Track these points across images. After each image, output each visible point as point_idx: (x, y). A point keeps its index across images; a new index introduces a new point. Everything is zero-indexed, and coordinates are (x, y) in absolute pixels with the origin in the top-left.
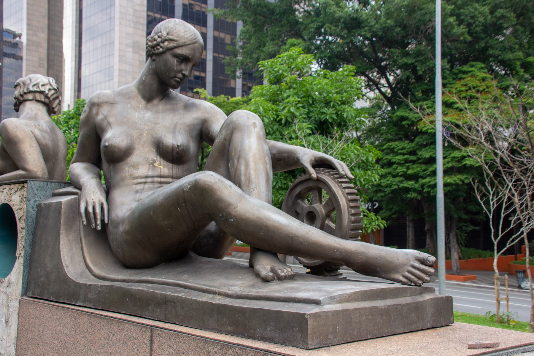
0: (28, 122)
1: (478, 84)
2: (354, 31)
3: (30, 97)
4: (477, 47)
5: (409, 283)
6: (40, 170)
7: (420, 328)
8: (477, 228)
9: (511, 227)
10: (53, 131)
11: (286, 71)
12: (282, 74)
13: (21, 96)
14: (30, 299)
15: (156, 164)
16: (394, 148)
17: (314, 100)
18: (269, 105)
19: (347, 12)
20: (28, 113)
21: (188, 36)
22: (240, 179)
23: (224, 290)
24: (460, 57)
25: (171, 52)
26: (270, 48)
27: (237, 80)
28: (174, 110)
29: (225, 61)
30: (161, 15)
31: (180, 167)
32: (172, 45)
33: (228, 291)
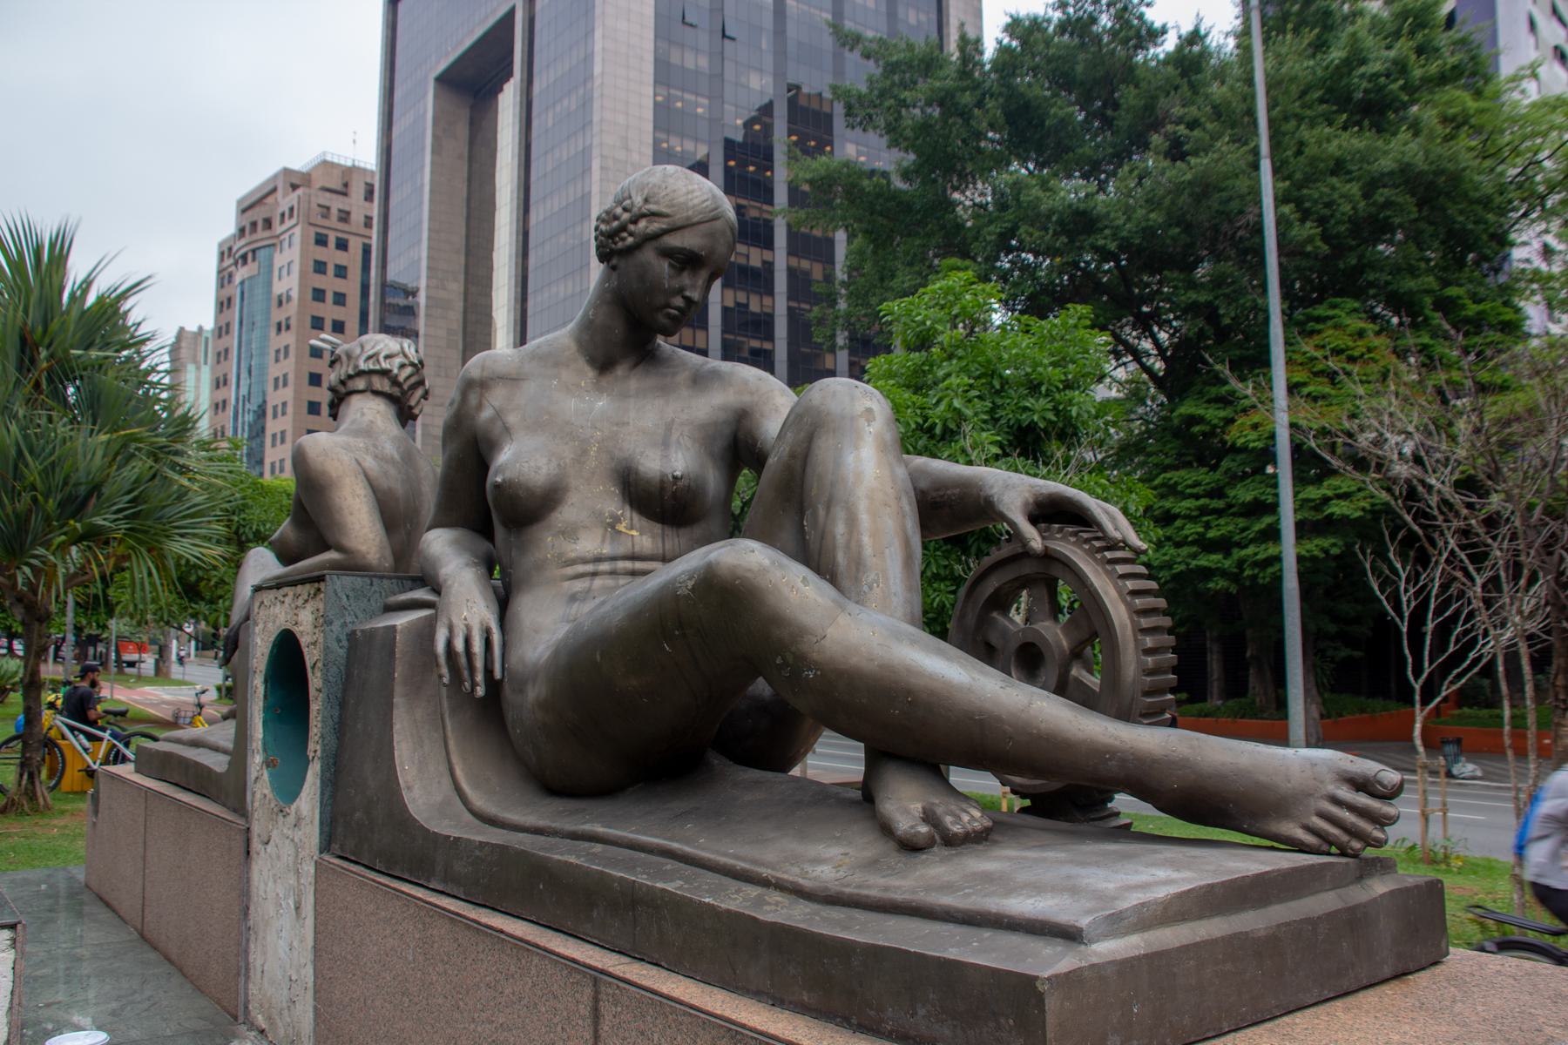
0: (351, 440)
1: (1350, 344)
2: (1082, 238)
3: (360, 384)
4: (1342, 266)
5: (1325, 847)
6: (374, 549)
7: (1365, 982)
8: (1357, 654)
9: (1451, 650)
11: (939, 321)
13: (343, 383)
14: (337, 861)
15: (621, 527)
16: (1176, 484)
17: (1005, 382)
18: (906, 395)
19: (1064, 199)
20: (353, 422)
21: (696, 201)
22: (834, 557)
23: (791, 874)
24: (1324, 279)
25: (654, 244)
26: (904, 278)
27: (839, 353)
28: (665, 391)
29: (813, 315)
31: (683, 531)
32: (656, 226)
33: (801, 881)
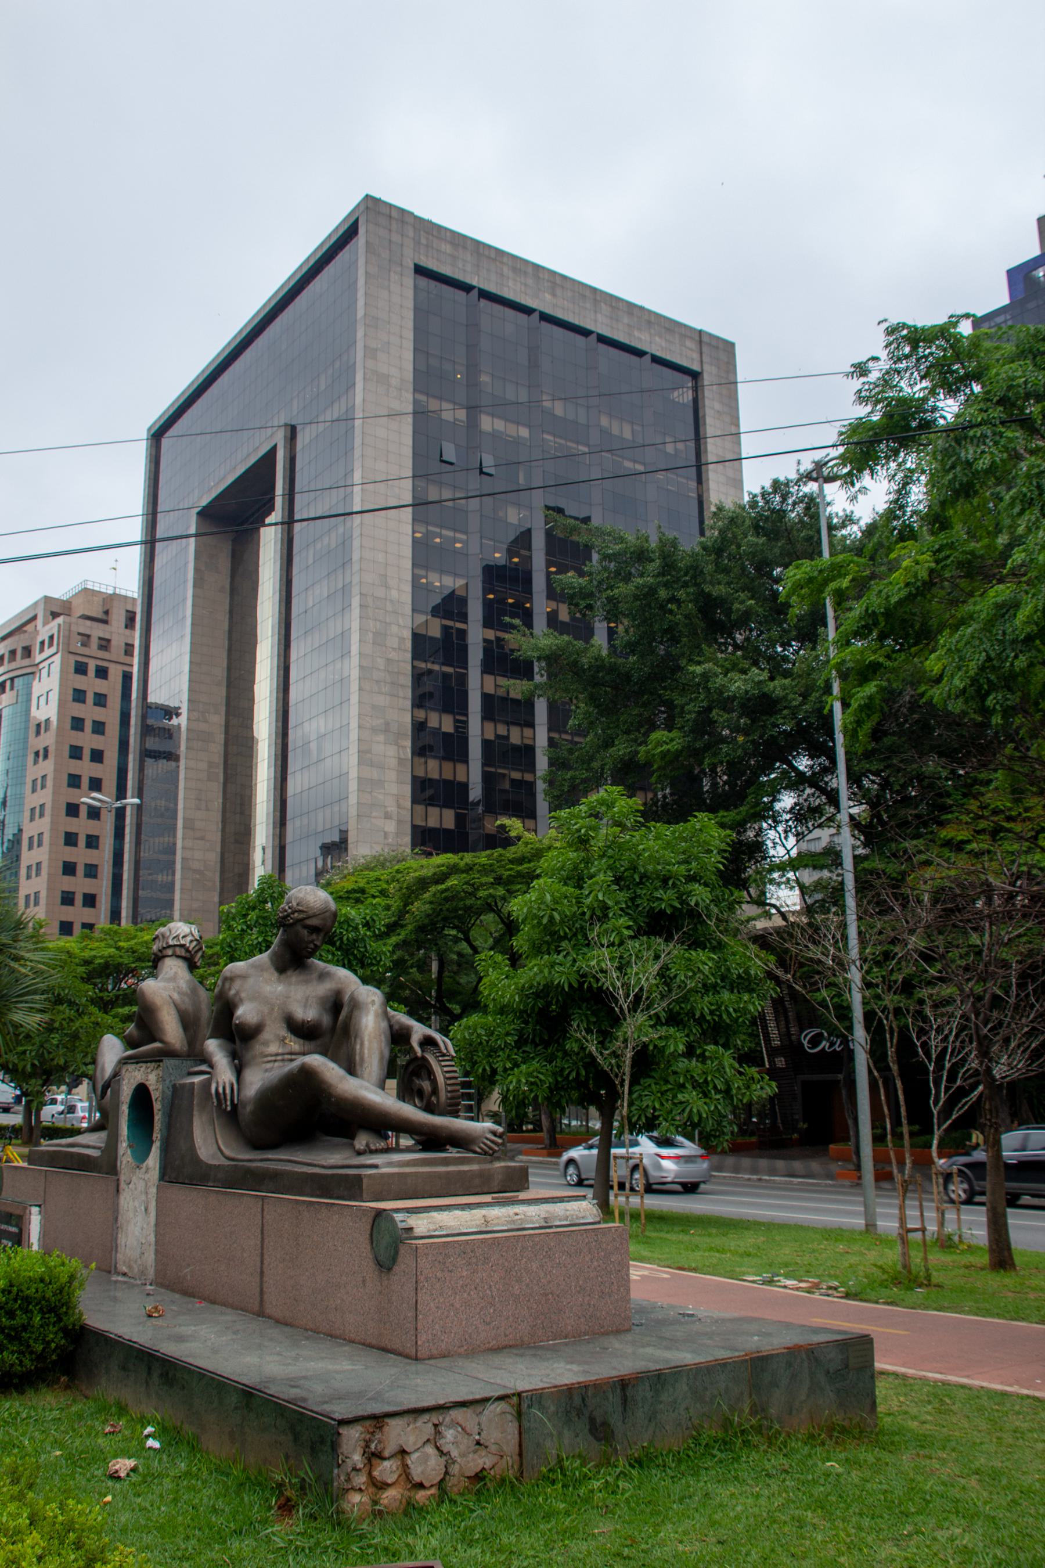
3: (170, 952)
10: (194, 991)
12: (586, 834)
28: (307, 982)
32: (301, 916)
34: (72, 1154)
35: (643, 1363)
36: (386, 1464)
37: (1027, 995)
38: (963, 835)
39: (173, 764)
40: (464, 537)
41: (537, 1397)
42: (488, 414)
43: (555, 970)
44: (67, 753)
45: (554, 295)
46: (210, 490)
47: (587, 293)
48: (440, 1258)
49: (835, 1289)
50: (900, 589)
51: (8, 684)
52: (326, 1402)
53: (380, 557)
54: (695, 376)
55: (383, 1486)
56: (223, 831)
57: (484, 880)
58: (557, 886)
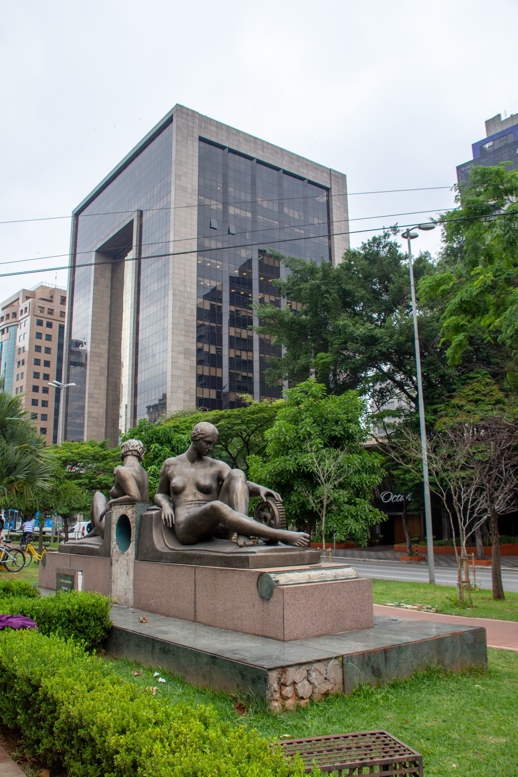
3: (130, 453)
10: (142, 472)
28: (205, 467)
30: (210, 322)
32: (203, 436)
34: (83, 547)
35: (390, 642)
36: (288, 688)
37: (510, 475)
38: (463, 403)
39: (83, 368)
40: (221, 263)
41: (350, 657)
42: (232, 206)
43: (288, 463)
44: (33, 362)
45: (263, 151)
46: (102, 240)
47: (279, 151)
48: (293, 594)
49: (430, 609)
50: (477, 289)
51: (6, 330)
52: (256, 661)
53: (182, 272)
54: (328, 190)
55: (287, 698)
56: (107, 399)
57: (236, 422)
58: (287, 424)
